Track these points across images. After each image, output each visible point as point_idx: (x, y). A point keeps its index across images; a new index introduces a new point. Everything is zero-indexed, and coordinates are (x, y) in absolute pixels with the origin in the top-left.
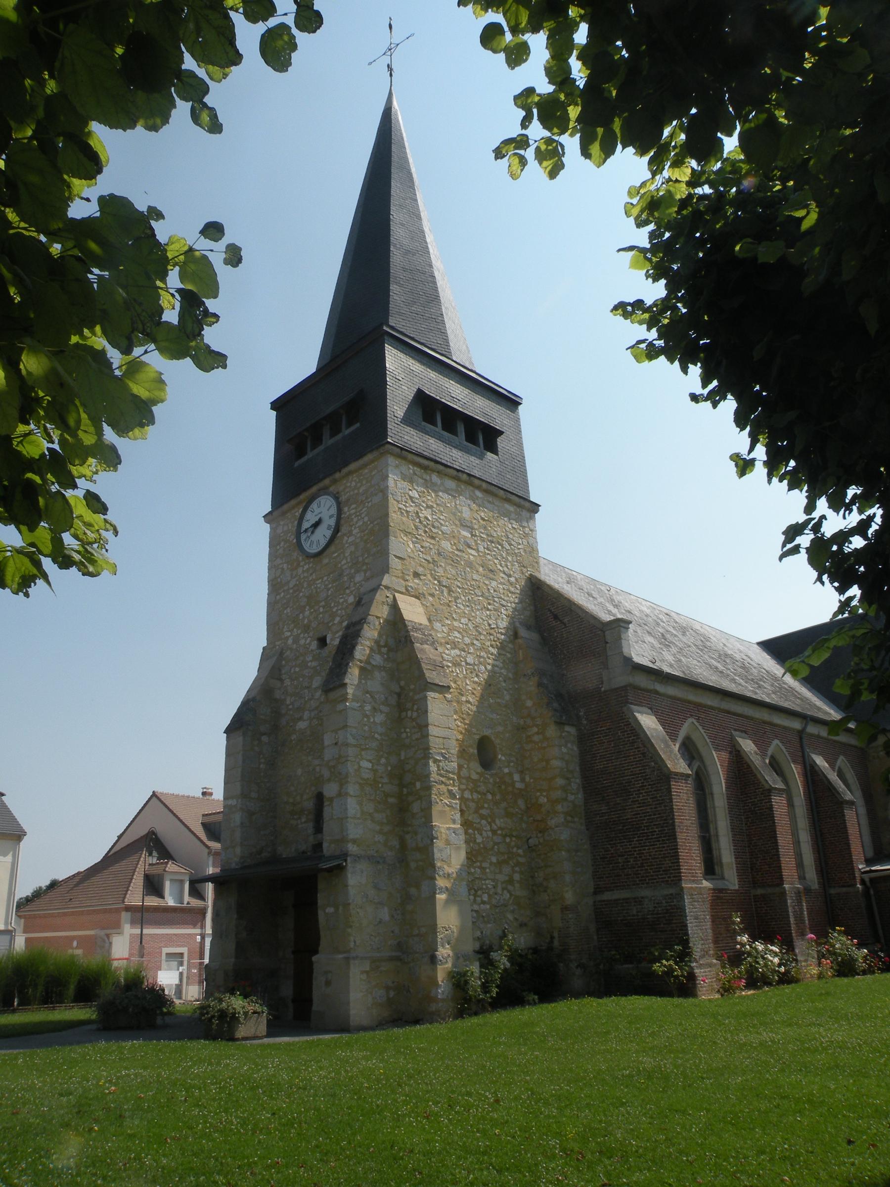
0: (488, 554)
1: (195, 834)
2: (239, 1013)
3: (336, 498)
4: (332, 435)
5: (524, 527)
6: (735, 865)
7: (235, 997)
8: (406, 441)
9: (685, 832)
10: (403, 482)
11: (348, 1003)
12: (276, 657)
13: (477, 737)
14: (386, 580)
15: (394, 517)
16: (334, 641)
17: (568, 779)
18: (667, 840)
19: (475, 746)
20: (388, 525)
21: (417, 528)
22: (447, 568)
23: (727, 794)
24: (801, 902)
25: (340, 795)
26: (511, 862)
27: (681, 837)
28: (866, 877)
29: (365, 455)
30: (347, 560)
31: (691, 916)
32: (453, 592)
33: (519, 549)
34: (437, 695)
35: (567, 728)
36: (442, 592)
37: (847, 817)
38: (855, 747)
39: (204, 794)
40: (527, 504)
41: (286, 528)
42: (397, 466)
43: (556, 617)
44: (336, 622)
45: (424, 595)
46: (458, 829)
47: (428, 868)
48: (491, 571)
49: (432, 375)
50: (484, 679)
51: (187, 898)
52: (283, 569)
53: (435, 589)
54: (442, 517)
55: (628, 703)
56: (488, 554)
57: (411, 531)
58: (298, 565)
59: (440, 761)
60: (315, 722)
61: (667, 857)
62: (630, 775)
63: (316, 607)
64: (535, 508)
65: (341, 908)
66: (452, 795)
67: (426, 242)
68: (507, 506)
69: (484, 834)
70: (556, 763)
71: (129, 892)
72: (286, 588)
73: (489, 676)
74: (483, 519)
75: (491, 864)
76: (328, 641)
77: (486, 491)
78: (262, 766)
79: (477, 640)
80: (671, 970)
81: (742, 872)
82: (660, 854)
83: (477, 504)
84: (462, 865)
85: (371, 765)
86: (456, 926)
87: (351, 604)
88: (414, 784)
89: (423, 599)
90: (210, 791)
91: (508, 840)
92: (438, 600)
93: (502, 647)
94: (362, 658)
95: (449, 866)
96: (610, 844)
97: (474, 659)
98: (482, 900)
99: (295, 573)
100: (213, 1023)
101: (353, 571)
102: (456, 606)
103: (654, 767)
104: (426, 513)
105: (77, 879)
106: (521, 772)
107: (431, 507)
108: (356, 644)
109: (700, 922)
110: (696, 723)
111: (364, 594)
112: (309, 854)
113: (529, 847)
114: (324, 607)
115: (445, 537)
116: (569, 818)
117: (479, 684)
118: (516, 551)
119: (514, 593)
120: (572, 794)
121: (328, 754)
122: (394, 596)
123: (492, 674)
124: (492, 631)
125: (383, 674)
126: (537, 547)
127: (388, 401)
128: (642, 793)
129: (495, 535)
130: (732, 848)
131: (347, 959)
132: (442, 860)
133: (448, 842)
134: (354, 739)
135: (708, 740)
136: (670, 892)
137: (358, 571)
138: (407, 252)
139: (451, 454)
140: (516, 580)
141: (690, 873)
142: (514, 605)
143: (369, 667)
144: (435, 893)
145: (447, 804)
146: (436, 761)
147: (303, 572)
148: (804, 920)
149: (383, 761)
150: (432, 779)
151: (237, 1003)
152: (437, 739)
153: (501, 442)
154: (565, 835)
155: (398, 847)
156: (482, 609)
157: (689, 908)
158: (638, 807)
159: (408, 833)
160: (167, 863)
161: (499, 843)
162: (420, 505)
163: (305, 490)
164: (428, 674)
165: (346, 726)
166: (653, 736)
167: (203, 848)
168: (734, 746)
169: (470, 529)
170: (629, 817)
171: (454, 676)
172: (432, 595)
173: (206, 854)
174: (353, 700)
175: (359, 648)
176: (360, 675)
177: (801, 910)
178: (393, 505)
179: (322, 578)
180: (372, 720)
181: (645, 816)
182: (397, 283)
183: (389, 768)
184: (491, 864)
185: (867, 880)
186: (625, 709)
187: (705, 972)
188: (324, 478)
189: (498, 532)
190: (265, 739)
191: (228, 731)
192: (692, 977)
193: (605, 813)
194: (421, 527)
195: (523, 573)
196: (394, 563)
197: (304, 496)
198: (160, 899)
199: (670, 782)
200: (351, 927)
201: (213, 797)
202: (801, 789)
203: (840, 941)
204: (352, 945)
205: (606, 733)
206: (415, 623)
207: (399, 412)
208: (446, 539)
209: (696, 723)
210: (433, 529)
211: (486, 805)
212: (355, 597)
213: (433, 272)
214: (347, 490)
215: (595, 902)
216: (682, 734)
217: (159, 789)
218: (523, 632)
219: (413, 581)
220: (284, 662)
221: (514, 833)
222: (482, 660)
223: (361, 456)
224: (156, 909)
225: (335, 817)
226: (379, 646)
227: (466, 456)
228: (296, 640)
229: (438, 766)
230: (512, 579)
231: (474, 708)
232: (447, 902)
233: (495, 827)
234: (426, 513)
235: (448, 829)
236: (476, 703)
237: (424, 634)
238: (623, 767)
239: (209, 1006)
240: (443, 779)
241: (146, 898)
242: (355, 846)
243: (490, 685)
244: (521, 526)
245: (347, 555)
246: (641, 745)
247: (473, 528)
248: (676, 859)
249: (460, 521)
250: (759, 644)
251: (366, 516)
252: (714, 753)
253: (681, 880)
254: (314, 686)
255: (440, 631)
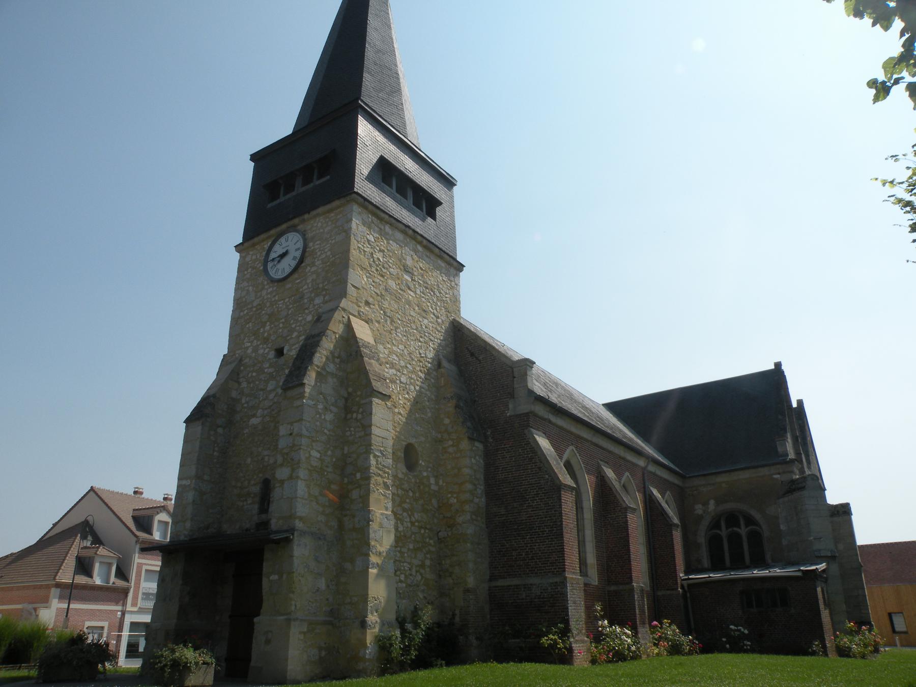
0: (423, 297)
1: (125, 525)
2: (191, 663)
3: (304, 235)
4: (304, 184)
5: (451, 281)
6: (596, 566)
7: (187, 648)
8: (368, 195)
9: (569, 533)
10: (363, 227)
11: (287, 659)
12: (236, 363)
13: (405, 443)
14: (344, 303)
15: (354, 253)
16: (291, 352)
17: (475, 485)
18: (555, 538)
19: (403, 451)
20: (349, 259)
21: (371, 266)
22: (391, 302)
23: (594, 509)
24: (644, 598)
25: (291, 478)
26: (424, 550)
27: (566, 536)
28: (685, 583)
29: (332, 201)
30: (308, 286)
31: (571, 601)
32: (394, 322)
33: (446, 297)
34: (379, 401)
35: (477, 444)
36: (386, 321)
37: (674, 537)
38: (678, 486)
39: (135, 492)
40: (455, 263)
41: (254, 257)
42: (359, 213)
43: (472, 355)
44: (293, 336)
45: (372, 321)
46: (389, 515)
47: (363, 545)
48: (424, 311)
49: (391, 147)
50: (413, 397)
51: (113, 578)
52: (248, 290)
53: (381, 317)
54: (390, 261)
55: (529, 426)
56: (423, 297)
57: (366, 267)
58: (263, 289)
59: (378, 457)
60: (268, 419)
61: (555, 552)
62: (527, 485)
63: (277, 323)
64: (460, 267)
65: (285, 576)
66: (386, 486)
67: (393, 47)
68: (440, 262)
69: (405, 523)
70: (466, 471)
71: (61, 571)
72: (249, 307)
73: (417, 395)
74: (421, 268)
75: (409, 549)
76: (285, 351)
77: (425, 247)
78: (215, 453)
79: (410, 364)
80: (556, 643)
81: (600, 573)
82: (549, 550)
83: (417, 256)
84: (391, 546)
85: (319, 455)
86: (383, 597)
87: (309, 322)
88: (355, 475)
89: (371, 324)
90: (141, 490)
91: (422, 531)
92: (382, 327)
93: (428, 374)
94: (319, 364)
95: (381, 545)
96: (505, 540)
97: (407, 379)
98: (400, 579)
99: (259, 294)
100: (165, 672)
101: (313, 295)
102: (396, 334)
103: (548, 479)
104: (378, 255)
105: (8, 560)
106: (436, 477)
107: (383, 251)
108: (315, 352)
109: (577, 606)
110: (575, 450)
111: (323, 313)
112: (252, 531)
113: (438, 539)
114: (283, 323)
115: (392, 277)
116: (474, 517)
117: (409, 400)
118: (444, 299)
119: (441, 332)
120: (477, 498)
121: (282, 443)
122: (349, 318)
123: (420, 393)
124: (422, 359)
125: (335, 380)
126: (459, 298)
127: (357, 160)
128: (536, 500)
129: (430, 283)
130: (595, 552)
131: (288, 621)
132: (376, 540)
133: (381, 526)
134: (307, 431)
135: (582, 465)
136: (556, 581)
137: (317, 295)
138: (379, 51)
139: (401, 213)
140: (443, 321)
141: (571, 566)
142: (439, 341)
143: (324, 373)
144: (368, 568)
145: (382, 494)
146: (375, 456)
147: (267, 294)
148: (645, 612)
149: (329, 453)
150: (371, 471)
151: (189, 654)
152: (378, 438)
153: (439, 211)
154: (470, 530)
155: (336, 527)
156: (415, 340)
157: (570, 594)
158: (532, 511)
159: (346, 516)
160: (98, 548)
161: (416, 533)
162: (375, 247)
163: (276, 226)
164: (374, 383)
165: (301, 420)
166: (547, 454)
167: (132, 536)
168: (600, 472)
169: (411, 274)
170: (524, 518)
171: (393, 389)
172: (378, 322)
173: (135, 542)
174: (309, 398)
175: (317, 355)
176: (316, 378)
177: (643, 603)
178: (354, 243)
179: (284, 300)
180: (323, 417)
181: (538, 519)
182: (369, 73)
183: (334, 460)
184: (409, 549)
185: (686, 586)
186: (526, 431)
187: (579, 647)
188: (294, 217)
189: (432, 281)
190: (220, 430)
191: (188, 421)
192: (570, 650)
193: (504, 514)
194: (374, 266)
195: (448, 317)
196: (351, 290)
197: (273, 232)
198: (90, 579)
199: (560, 491)
200: (293, 592)
201: (143, 496)
202: (642, 513)
203: (671, 630)
204: (293, 608)
205: (508, 450)
206: (365, 341)
207: (364, 171)
208: (392, 279)
209: (575, 450)
210: (383, 269)
211: (408, 501)
212: (313, 316)
213: (397, 70)
214: (314, 229)
215: (490, 587)
216: (565, 457)
217: (97, 485)
218: (445, 363)
219: (364, 308)
220: (242, 368)
221: (428, 527)
222: (412, 381)
223: (329, 202)
224: (84, 587)
225: (285, 497)
226: (334, 357)
227: (412, 216)
228: (255, 350)
229: (377, 461)
230: (439, 320)
231: (404, 420)
232: (378, 576)
233: (413, 519)
234: (378, 255)
235: (382, 514)
236: (406, 416)
237: (371, 352)
238: (522, 478)
239: (162, 656)
240: (381, 472)
241: (76, 577)
242: (301, 523)
243: (417, 402)
244: (449, 280)
245: (308, 281)
246: (538, 462)
247: (413, 274)
248: (562, 554)
249: (404, 266)
250: (603, 405)
251: (329, 250)
252: (586, 475)
253: (565, 571)
254: (268, 389)
255: (383, 351)
